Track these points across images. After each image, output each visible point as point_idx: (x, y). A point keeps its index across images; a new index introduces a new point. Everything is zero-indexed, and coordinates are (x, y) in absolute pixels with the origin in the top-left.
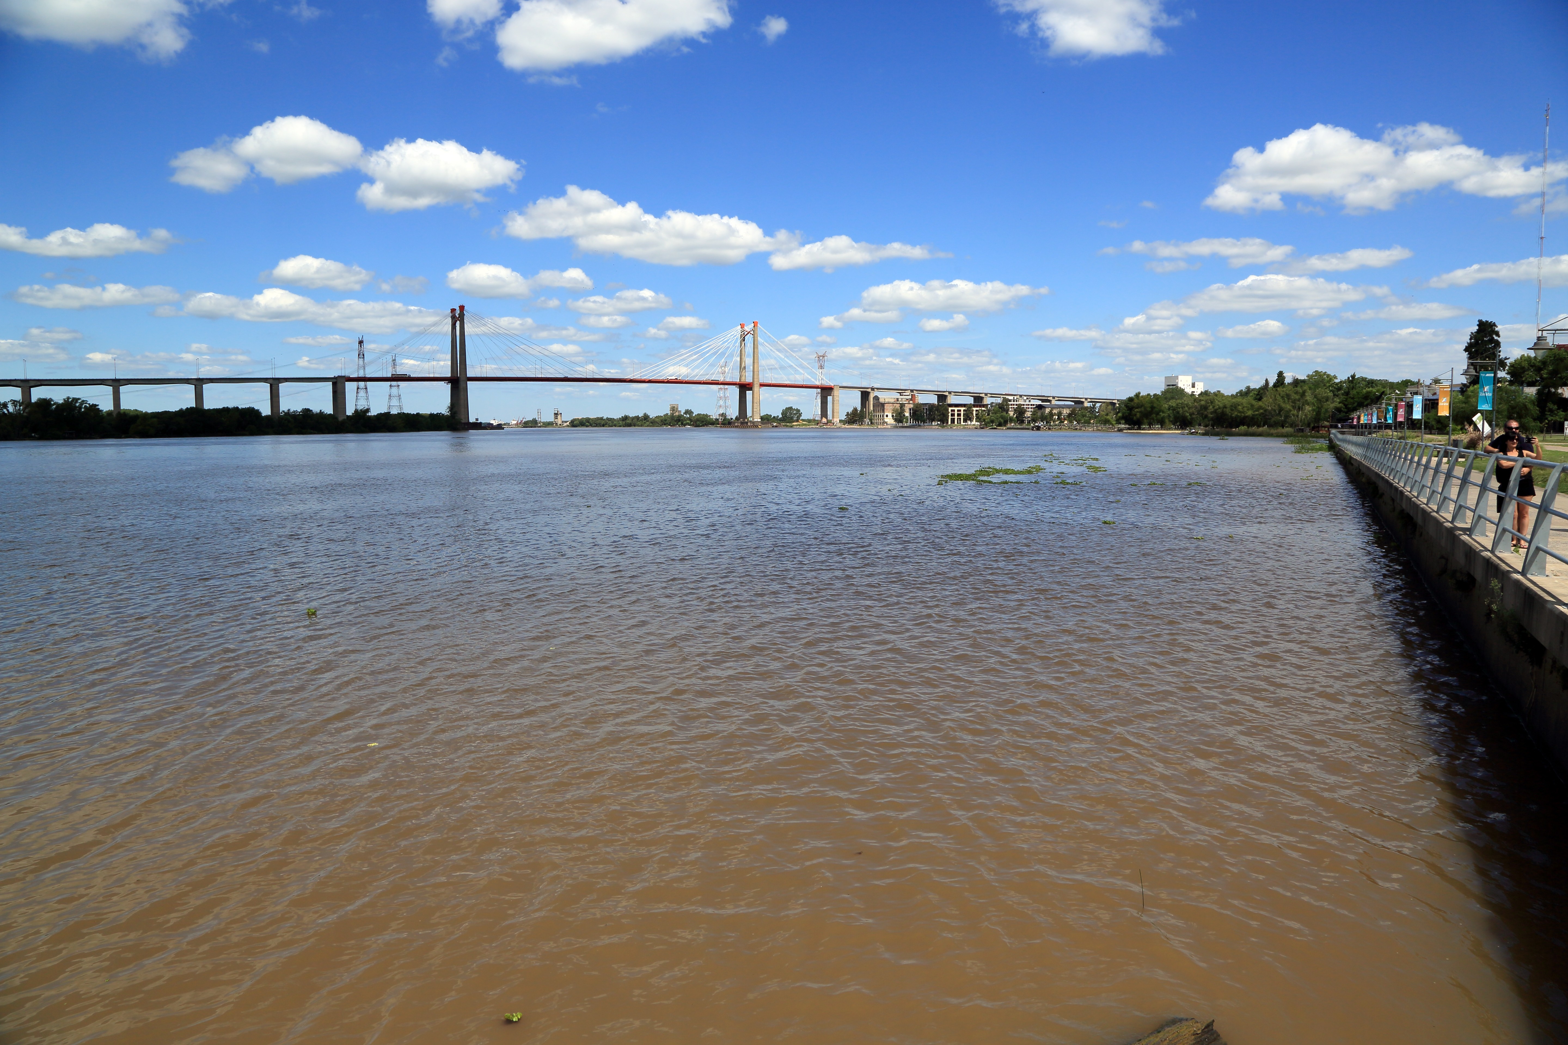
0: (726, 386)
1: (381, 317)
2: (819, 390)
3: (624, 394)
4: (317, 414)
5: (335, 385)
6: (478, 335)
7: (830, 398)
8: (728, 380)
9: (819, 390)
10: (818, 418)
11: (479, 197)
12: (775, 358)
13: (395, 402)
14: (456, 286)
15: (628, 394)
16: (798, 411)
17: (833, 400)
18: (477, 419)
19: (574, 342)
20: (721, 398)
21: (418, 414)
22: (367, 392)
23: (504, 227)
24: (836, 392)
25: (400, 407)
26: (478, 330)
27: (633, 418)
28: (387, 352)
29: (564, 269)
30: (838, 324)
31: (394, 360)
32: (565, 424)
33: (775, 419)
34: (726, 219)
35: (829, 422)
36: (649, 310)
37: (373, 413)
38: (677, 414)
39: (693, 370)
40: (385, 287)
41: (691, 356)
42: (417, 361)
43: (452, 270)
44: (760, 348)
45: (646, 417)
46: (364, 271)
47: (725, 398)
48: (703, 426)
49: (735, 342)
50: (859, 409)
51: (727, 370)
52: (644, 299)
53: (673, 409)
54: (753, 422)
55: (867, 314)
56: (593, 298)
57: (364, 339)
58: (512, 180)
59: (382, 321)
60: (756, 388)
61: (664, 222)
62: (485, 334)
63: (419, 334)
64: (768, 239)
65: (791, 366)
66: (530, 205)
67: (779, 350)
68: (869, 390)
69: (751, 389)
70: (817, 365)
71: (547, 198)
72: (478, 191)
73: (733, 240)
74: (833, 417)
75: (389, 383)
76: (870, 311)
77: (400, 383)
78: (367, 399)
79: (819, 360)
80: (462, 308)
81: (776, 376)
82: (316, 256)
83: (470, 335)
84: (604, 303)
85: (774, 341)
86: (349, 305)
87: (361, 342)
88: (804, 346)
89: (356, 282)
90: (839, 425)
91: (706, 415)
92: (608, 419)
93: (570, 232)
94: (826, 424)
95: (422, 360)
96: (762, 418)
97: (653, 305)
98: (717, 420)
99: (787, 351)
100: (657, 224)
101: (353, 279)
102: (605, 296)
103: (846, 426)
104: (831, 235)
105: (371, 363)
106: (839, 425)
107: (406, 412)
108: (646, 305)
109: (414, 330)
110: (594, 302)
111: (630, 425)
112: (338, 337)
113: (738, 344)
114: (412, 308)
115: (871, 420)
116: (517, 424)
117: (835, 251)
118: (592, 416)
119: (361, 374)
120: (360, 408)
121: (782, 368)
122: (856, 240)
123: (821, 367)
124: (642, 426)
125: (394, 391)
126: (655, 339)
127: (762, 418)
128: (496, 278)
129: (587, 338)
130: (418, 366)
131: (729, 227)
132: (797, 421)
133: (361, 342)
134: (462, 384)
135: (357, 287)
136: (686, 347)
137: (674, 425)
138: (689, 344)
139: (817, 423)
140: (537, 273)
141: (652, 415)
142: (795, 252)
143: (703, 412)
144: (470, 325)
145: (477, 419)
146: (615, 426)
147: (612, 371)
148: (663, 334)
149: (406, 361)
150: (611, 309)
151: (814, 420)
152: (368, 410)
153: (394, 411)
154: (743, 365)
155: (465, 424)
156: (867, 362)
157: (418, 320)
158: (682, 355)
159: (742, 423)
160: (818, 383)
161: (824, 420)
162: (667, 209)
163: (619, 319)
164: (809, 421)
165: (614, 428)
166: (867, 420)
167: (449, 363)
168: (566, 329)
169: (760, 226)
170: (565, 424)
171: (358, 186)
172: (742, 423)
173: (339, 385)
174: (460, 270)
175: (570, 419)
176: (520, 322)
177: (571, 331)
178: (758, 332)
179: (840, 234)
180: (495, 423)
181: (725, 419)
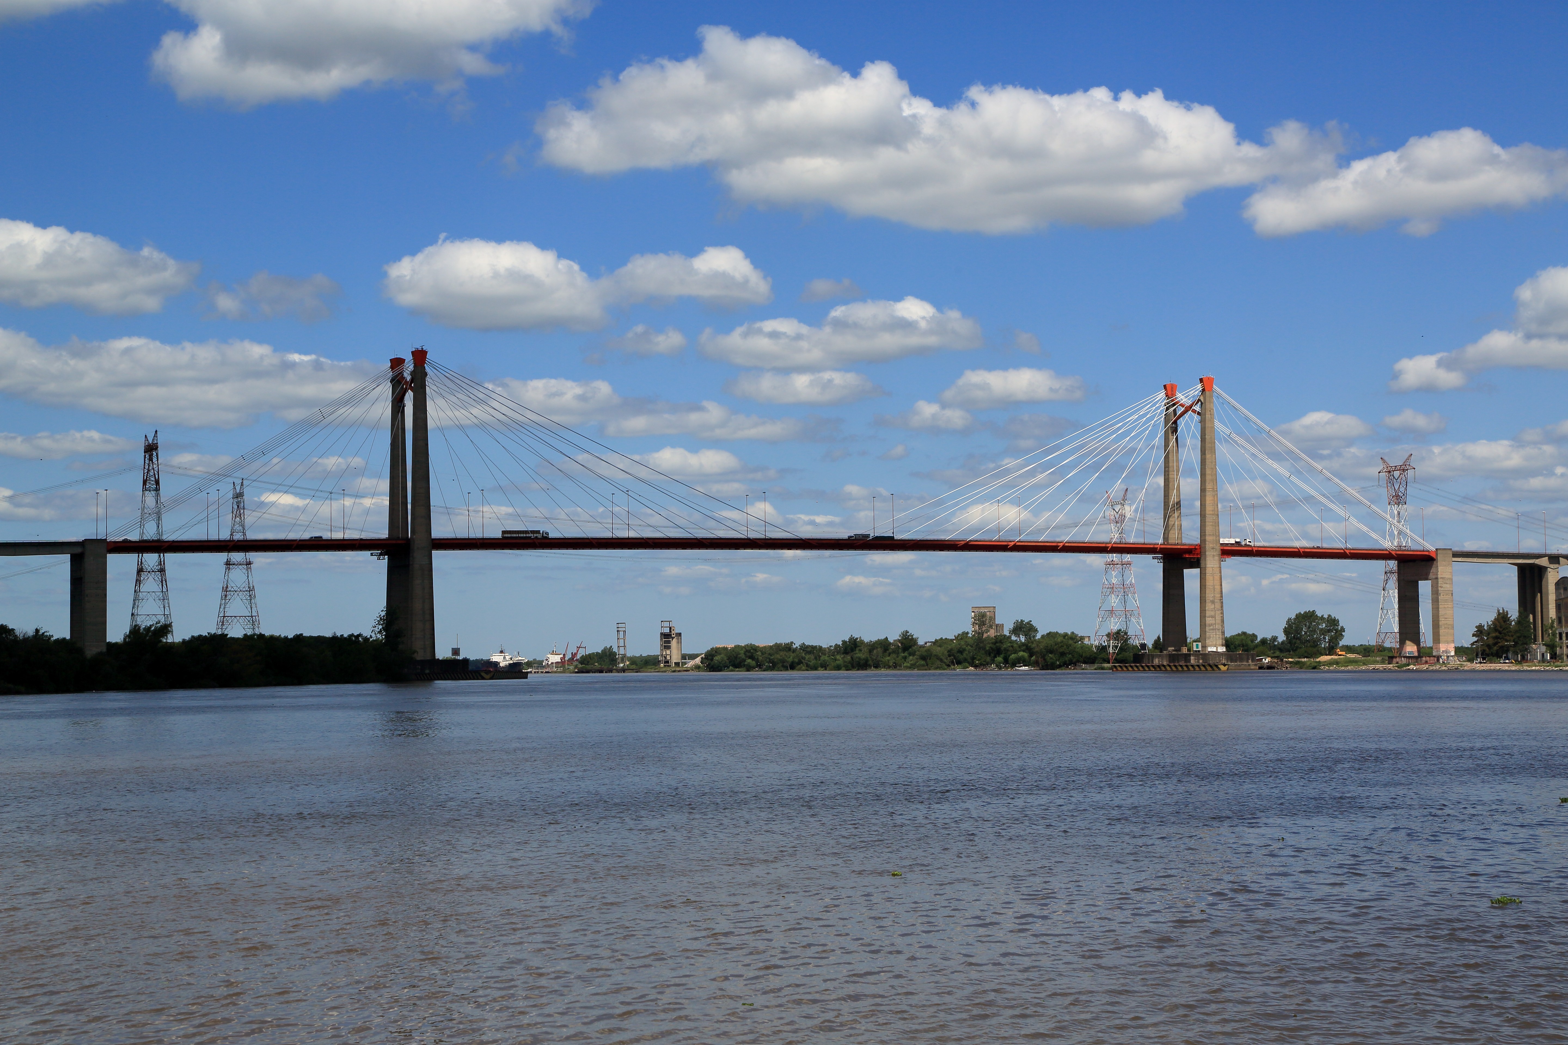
0: (1128, 557)
1: (212, 381)
2: (1393, 564)
3: (848, 579)
4: (26, 640)
5: (77, 561)
6: (461, 427)
7: (1424, 587)
8: (1132, 539)
9: (1393, 564)
10: (1391, 642)
11: (473, 64)
12: (1265, 478)
13: (237, 606)
14: (408, 298)
15: (859, 580)
16: (1333, 622)
17: (1435, 593)
18: (456, 651)
19: (717, 444)
20: (1112, 588)
21: (299, 638)
22: (163, 581)
23: (539, 143)
24: (1444, 569)
25: (253, 620)
26: (461, 415)
27: (873, 646)
28: (223, 474)
29: (694, 250)
30: (1450, 379)
31: (239, 496)
32: (691, 663)
33: (1267, 645)
34: (1128, 101)
35: (1424, 654)
36: (921, 352)
37: (179, 635)
38: (992, 633)
39: (1036, 513)
40: (226, 303)
41: (1032, 473)
42: (302, 496)
43: (398, 258)
44: (1222, 451)
45: (907, 643)
46: (171, 262)
47: (1125, 589)
48: (1065, 665)
49: (1152, 436)
50: (1514, 613)
51: (1128, 511)
52: (906, 325)
53: (982, 619)
54: (1205, 656)
55: (1535, 344)
56: (769, 325)
57: (160, 441)
58: (565, 22)
59: (212, 393)
60: (1211, 560)
61: (960, 117)
62: (482, 426)
63: (305, 425)
64: (1249, 150)
65: (1309, 499)
66: (606, 82)
67: (1276, 456)
68: (1544, 562)
69: (1196, 563)
70: (1384, 493)
71: (650, 61)
72: (473, 48)
73: (1149, 158)
74: (1437, 639)
75: (222, 557)
76: (1541, 336)
77: (253, 556)
78: (165, 598)
79: (1391, 480)
80: (420, 356)
81: (1268, 527)
82: (42, 223)
83: (441, 429)
84: (798, 337)
85: (1260, 430)
86: (127, 351)
87: (151, 449)
88: (1350, 441)
89: (151, 291)
90: (1455, 662)
91: (1073, 638)
92: (805, 648)
93: (710, 152)
94: (1417, 659)
95: (314, 494)
96: (1229, 643)
97: (932, 340)
98: (1103, 649)
99: (1297, 459)
100: (941, 123)
101: (143, 281)
102: (802, 320)
103: (1477, 666)
104: (1426, 130)
105: (177, 502)
106: (1455, 662)
107: (267, 633)
108: (914, 341)
109: (296, 415)
110: (774, 335)
111: (863, 665)
112: (95, 435)
113: (1159, 440)
114: (296, 357)
115: (1551, 647)
116: (562, 663)
117: (1440, 175)
118: (764, 639)
119: (150, 533)
120: (145, 622)
121: (1285, 504)
122: (1504, 141)
123: (1398, 499)
124: (895, 666)
125: (238, 576)
126: (935, 430)
127: (1229, 643)
128: (515, 276)
129: (753, 432)
130: (304, 510)
131: (1141, 122)
132: (1331, 650)
133: (151, 449)
134: (418, 558)
135: (152, 304)
136: (1016, 452)
137: (983, 665)
138: (1024, 444)
139: (1390, 656)
140: (624, 262)
141: (924, 637)
142: (1326, 184)
143: (1063, 627)
144: (441, 402)
145: (456, 651)
146: (825, 666)
147: (819, 519)
148: (956, 417)
149: (272, 498)
150: (815, 355)
151: (1381, 649)
152: (165, 629)
153: (236, 631)
154: (1173, 499)
155: (423, 663)
156: (1536, 483)
157: (309, 390)
158: (1007, 471)
159: (1173, 658)
160: (1388, 544)
161: (1410, 648)
162: (969, 83)
163: (838, 378)
164: (1366, 651)
165: (820, 672)
166: (1539, 649)
167: (386, 502)
168: (700, 409)
169: (1226, 114)
170: (691, 663)
171: (155, 42)
172: (1173, 658)
173: (89, 562)
174: (420, 257)
175: (703, 649)
176: (578, 390)
177: (714, 413)
178: (1215, 406)
179: (1453, 124)
180: (502, 660)
181: (1125, 647)
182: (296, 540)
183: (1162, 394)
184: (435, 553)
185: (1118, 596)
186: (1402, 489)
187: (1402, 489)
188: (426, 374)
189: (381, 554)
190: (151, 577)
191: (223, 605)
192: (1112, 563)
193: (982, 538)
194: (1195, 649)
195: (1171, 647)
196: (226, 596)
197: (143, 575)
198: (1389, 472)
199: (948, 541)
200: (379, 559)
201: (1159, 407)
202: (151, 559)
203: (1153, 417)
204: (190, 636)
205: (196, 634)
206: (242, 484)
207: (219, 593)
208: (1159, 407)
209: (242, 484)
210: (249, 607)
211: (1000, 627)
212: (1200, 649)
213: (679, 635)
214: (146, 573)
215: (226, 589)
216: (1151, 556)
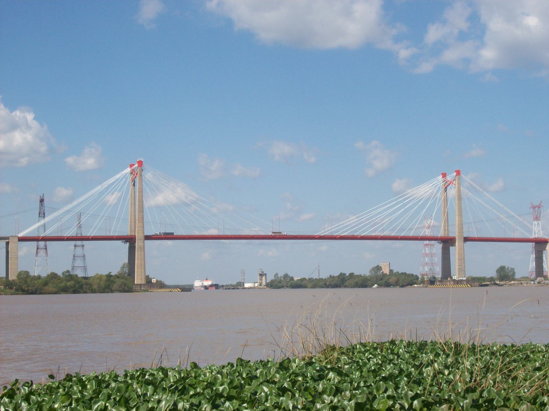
2: (532, 245)
9: (532, 245)
13: (79, 263)
75: (73, 243)
77: (85, 243)
125: (79, 251)
160: (533, 236)
183: (441, 176)
185: (429, 258)
186: (539, 215)
187: (539, 215)
189: (125, 242)
190: (42, 251)
191: (73, 262)
192: (427, 245)
193: (348, 234)
194: (453, 278)
196: (74, 259)
197: (39, 250)
198: (534, 208)
199: (373, 236)
200: (125, 244)
201: (440, 182)
202: (42, 244)
203: (438, 185)
206: (80, 215)
207: (72, 257)
208: (440, 182)
209: (80, 215)
210: (83, 263)
212: (455, 278)
213: (266, 274)
214: (40, 250)
215: (74, 256)
216: (437, 241)
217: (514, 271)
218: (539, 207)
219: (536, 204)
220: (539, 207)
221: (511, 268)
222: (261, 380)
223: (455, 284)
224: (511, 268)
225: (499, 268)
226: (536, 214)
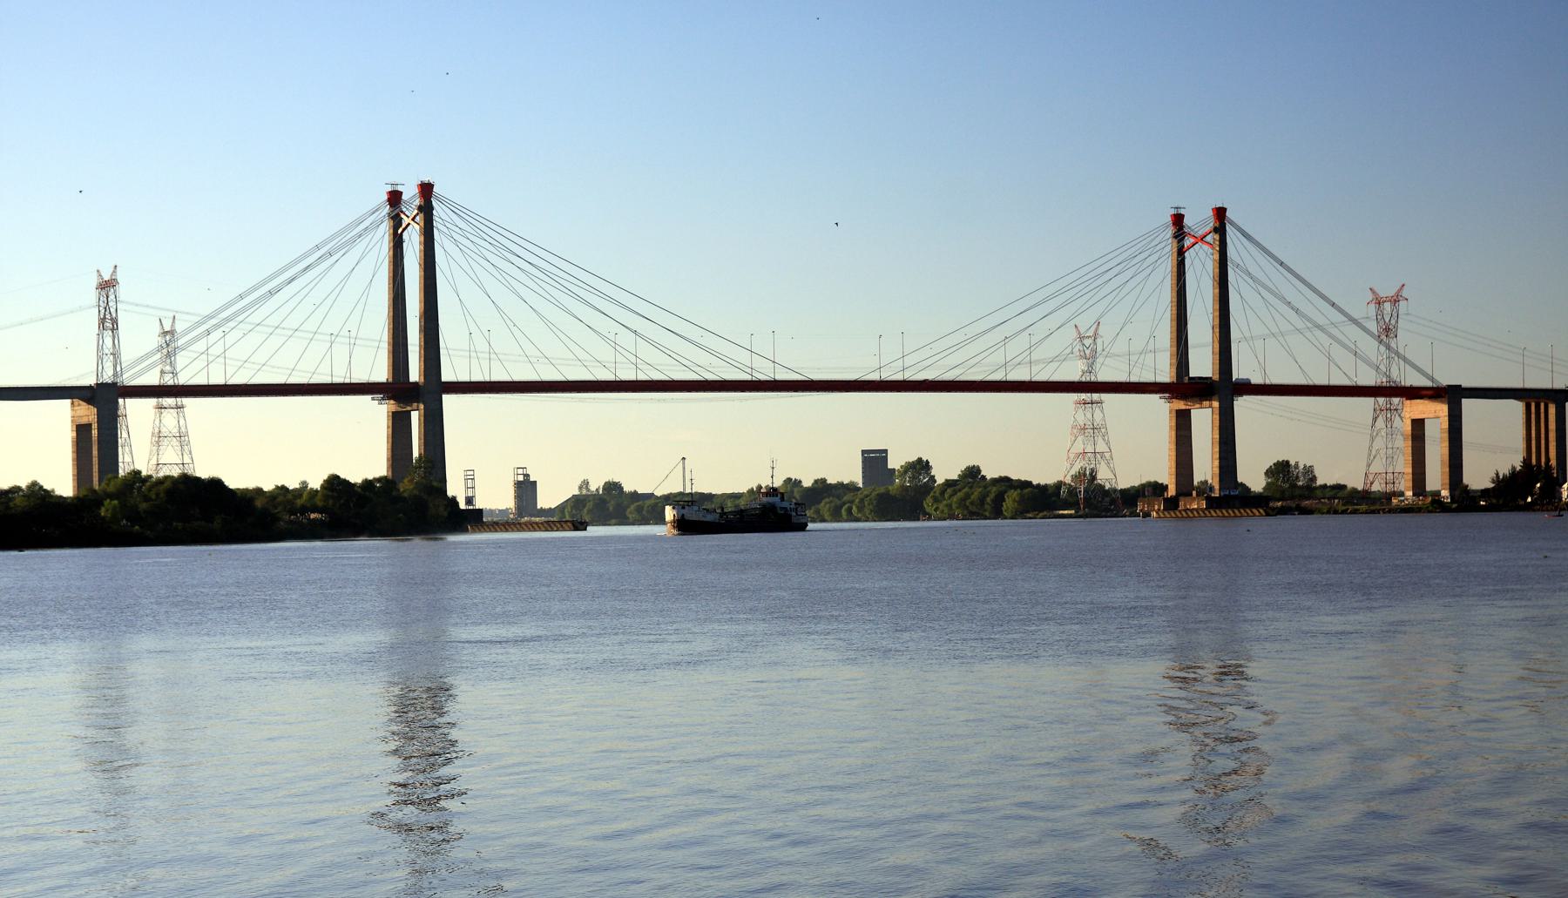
75: (152, 401)
77: (186, 401)
125: (170, 420)
182: (304, 384)
184: (445, 397)
186: (1393, 322)
187: (1393, 322)
188: (432, 209)
195: (1527, 498)
204: (812, 481)
205: (347, 479)
210: (180, 453)
211: (933, 479)
217: (1312, 472)
218: (1395, 300)
219: (1387, 291)
220: (1395, 300)
221: (1305, 466)
222: (980, 781)
223: (1212, 508)
224: (1305, 466)
225: (1274, 464)
226: (1387, 320)
